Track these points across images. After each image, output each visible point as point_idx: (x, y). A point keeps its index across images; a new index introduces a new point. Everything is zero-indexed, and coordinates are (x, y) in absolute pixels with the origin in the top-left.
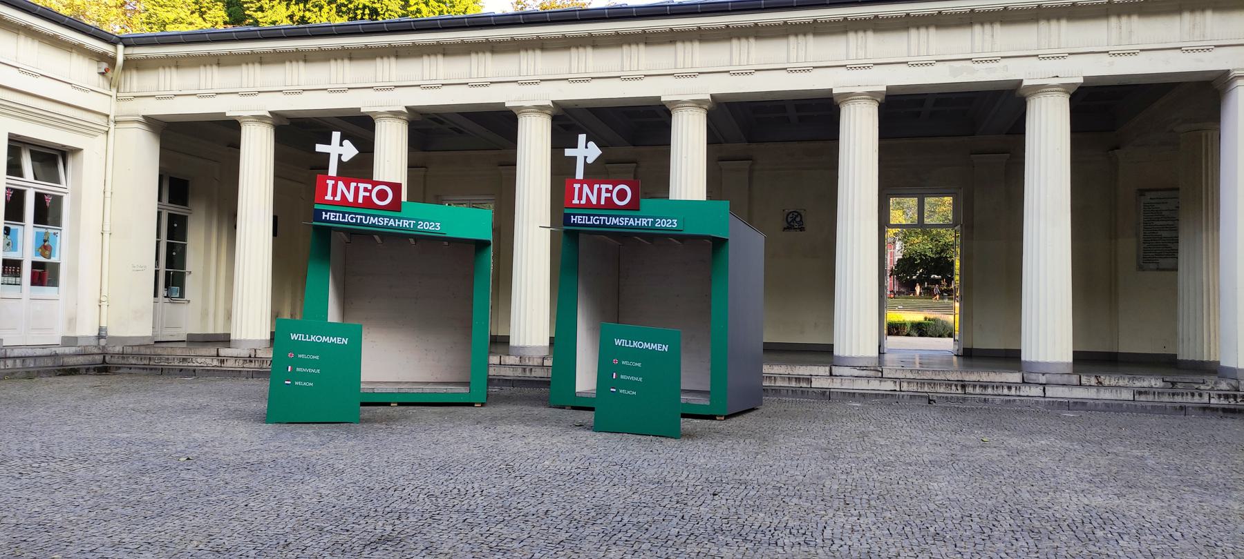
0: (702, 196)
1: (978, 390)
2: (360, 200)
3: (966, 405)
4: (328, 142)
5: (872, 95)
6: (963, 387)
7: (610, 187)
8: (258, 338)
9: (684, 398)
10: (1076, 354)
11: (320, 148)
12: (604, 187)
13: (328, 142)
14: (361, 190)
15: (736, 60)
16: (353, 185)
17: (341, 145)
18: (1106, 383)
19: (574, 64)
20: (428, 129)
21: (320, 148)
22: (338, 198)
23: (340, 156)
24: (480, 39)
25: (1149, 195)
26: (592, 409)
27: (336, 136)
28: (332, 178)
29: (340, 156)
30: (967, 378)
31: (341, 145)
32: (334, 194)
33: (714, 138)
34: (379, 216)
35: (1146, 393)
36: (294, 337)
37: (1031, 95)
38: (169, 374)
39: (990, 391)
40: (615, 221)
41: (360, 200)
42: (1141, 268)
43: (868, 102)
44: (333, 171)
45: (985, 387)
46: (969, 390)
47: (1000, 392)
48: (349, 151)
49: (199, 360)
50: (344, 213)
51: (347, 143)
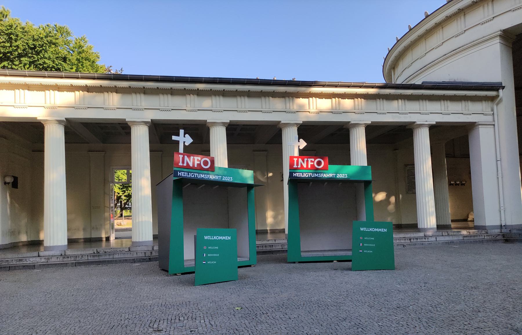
0: (226, 166)
1: (415, 240)
2: (309, 167)
3: (416, 246)
4: (178, 135)
5: (223, 124)
6: (410, 239)
7: (313, 160)
8: (59, 244)
9: (302, 254)
10: (437, 225)
11: (174, 138)
12: (310, 160)
13: (178, 135)
14: (309, 161)
15: (264, 106)
16: (306, 159)
17: (184, 137)
18: (450, 234)
19: (288, 105)
20: (237, 133)
21: (174, 138)
22: (185, 165)
23: (184, 142)
24: (67, 84)
25: (408, 167)
26: (350, 261)
27: (182, 132)
28: (181, 154)
29: (184, 142)
30: (406, 236)
31: (184, 137)
32: (183, 162)
33: (369, 142)
34: (205, 174)
35: (477, 236)
36: (206, 238)
37: (285, 127)
38: (15, 269)
39: (419, 240)
40: (202, 176)
41: (309, 167)
42: (407, 193)
43: (222, 127)
44: (181, 150)
45: (417, 239)
46: (412, 240)
47: (422, 240)
48: (189, 140)
49: (31, 259)
50: (188, 172)
51: (187, 135)
